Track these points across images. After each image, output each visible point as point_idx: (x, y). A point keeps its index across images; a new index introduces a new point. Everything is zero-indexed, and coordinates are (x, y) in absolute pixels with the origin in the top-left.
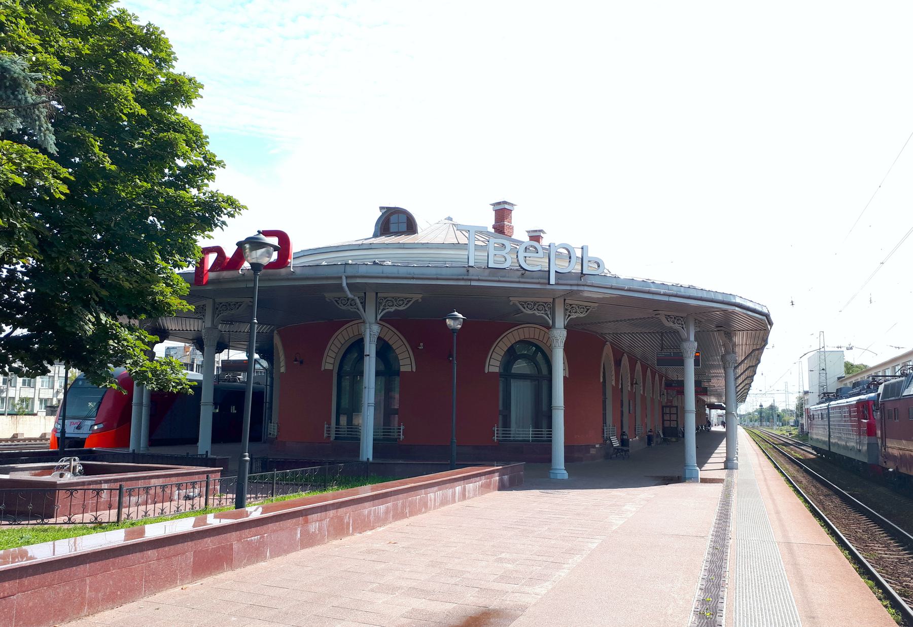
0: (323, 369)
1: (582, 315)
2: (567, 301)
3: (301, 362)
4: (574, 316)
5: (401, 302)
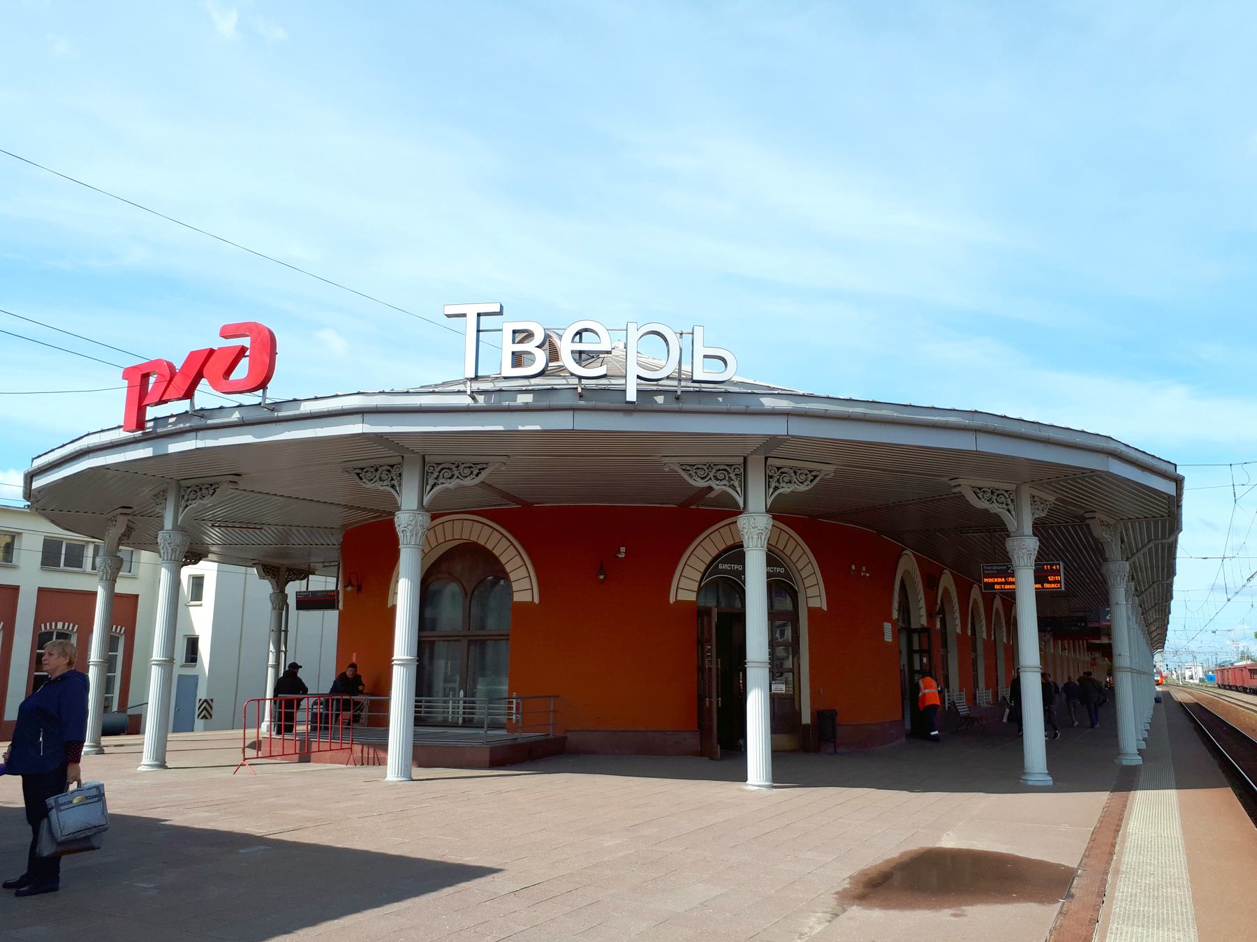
0: (672, 600)
1: (803, 488)
2: (770, 461)
3: (359, 589)
4: (786, 489)
5: (467, 471)
